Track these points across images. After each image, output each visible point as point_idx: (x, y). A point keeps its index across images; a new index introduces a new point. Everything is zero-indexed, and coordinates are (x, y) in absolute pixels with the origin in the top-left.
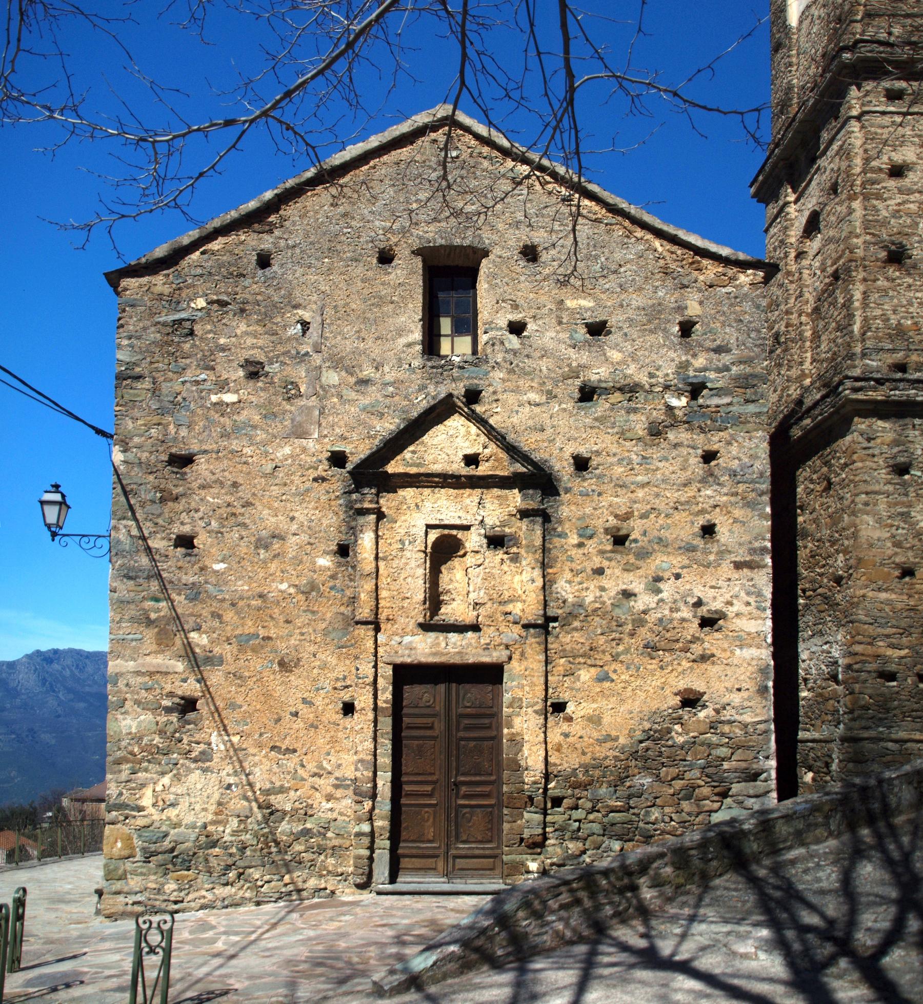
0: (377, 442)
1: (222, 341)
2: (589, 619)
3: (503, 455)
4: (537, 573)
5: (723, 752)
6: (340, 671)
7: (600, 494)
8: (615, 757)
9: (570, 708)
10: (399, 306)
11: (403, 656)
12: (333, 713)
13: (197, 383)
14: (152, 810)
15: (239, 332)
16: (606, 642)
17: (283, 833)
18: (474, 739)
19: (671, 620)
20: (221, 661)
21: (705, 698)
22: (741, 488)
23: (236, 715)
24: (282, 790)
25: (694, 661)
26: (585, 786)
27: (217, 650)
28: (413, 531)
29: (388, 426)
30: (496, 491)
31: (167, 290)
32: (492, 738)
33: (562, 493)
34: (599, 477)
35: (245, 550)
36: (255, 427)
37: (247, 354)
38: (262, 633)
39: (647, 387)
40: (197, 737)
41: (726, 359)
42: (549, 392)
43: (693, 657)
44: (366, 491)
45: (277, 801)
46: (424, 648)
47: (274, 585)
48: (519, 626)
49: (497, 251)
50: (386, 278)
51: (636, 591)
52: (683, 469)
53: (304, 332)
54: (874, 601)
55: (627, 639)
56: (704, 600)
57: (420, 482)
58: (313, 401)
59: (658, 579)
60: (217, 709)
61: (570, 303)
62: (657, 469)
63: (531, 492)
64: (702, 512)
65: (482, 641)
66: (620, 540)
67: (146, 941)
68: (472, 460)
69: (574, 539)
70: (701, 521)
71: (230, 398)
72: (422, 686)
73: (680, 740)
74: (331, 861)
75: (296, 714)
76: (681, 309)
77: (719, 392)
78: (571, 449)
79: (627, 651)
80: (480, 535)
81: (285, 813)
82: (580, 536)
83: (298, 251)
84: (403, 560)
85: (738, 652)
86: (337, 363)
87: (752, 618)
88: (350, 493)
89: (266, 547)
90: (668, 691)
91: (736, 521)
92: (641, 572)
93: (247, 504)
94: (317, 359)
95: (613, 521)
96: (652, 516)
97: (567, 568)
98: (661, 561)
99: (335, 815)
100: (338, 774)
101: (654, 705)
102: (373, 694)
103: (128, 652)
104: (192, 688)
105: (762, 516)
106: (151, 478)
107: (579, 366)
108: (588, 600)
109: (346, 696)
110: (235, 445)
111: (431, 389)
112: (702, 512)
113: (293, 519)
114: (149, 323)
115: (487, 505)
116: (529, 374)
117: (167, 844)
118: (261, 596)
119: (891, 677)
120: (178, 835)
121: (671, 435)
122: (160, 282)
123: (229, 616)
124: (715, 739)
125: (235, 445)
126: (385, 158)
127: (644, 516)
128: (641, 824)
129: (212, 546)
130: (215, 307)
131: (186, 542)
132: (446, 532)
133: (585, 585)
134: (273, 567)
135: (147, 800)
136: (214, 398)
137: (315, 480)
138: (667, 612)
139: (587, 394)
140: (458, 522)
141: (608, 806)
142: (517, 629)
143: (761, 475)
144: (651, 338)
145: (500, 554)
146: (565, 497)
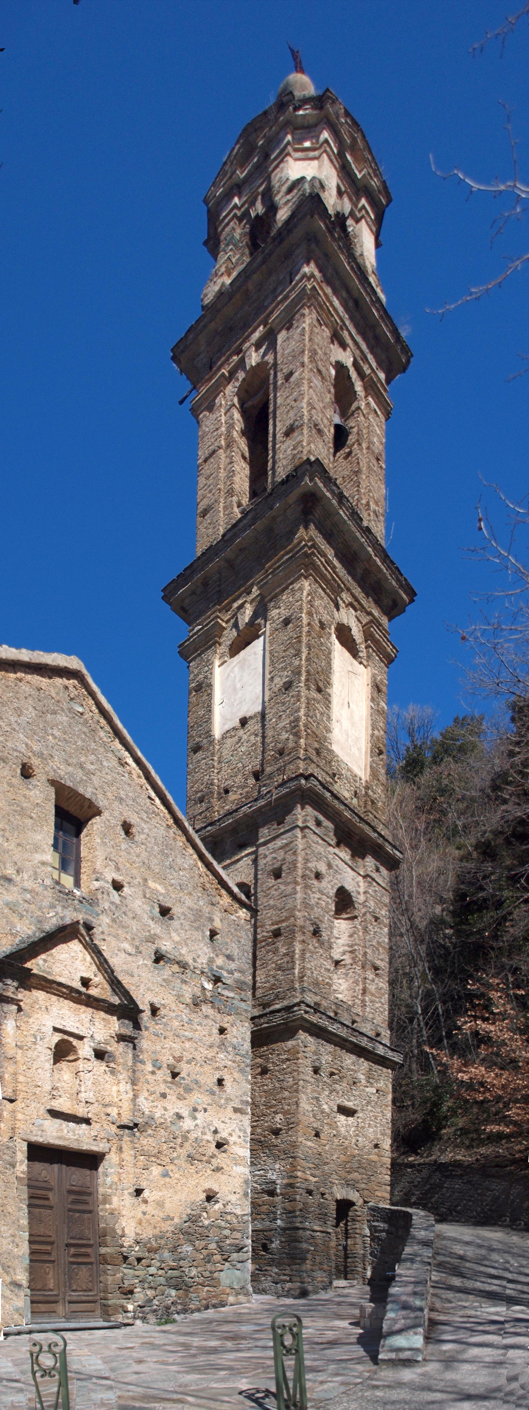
0: (17, 941)
2: (158, 1129)
3: (107, 986)
4: (129, 1087)
5: (227, 1232)
7: (165, 1038)
8: (172, 1231)
9: (146, 1194)
11: (37, 1136)
16: (167, 1149)
18: (79, 1211)
19: (202, 1140)
21: (218, 1196)
22: (238, 1058)
25: (213, 1170)
26: (155, 1251)
30: (102, 1014)
32: (90, 1212)
33: (143, 1029)
34: (165, 1025)
39: (192, 967)
41: (233, 966)
42: (137, 948)
43: (212, 1168)
48: (115, 1127)
49: (106, 815)
50: (27, 792)
51: (184, 1115)
54: (305, 1146)
56: (219, 1130)
57: (51, 988)
59: (195, 1110)
61: (151, 884)
62: (196, 1030)
63: (127, 1022)
64: (218, 1068)
65: (93, 1134)
66: (175, 1075)
67: (39, 1365)
68: (86, 982)
69: (149, 1067)
72: (41, 1164)
73: (206, 1222)
76: (211, 920)
80: (90, 1047)
82: (154, 1066)
84: (36, 1053)
85: (234, 1168)
90: (200, 1189)
91: (235, 1080)
95: (172, 1061)
96: (193, 1063)
97: (145, 1088)
98: (199, 1098)
105: (247, 1080)
107: (155, 935)
108: (157, 1115)
111: (59, 909)
112: (218, 1068)
115: (96, 1023)
116: (123, 927)
121: (204, 1008)
124: (223, 1224)
128: (186, 1279)
132: (66, 1037)
133: (155, 1104)
138: (200, 1134)
139: (159, 958)
140: (76, 1031)
141: (168, 1265)
142: (114, 1129)
144: (196, 933)
146: (144, 1033)
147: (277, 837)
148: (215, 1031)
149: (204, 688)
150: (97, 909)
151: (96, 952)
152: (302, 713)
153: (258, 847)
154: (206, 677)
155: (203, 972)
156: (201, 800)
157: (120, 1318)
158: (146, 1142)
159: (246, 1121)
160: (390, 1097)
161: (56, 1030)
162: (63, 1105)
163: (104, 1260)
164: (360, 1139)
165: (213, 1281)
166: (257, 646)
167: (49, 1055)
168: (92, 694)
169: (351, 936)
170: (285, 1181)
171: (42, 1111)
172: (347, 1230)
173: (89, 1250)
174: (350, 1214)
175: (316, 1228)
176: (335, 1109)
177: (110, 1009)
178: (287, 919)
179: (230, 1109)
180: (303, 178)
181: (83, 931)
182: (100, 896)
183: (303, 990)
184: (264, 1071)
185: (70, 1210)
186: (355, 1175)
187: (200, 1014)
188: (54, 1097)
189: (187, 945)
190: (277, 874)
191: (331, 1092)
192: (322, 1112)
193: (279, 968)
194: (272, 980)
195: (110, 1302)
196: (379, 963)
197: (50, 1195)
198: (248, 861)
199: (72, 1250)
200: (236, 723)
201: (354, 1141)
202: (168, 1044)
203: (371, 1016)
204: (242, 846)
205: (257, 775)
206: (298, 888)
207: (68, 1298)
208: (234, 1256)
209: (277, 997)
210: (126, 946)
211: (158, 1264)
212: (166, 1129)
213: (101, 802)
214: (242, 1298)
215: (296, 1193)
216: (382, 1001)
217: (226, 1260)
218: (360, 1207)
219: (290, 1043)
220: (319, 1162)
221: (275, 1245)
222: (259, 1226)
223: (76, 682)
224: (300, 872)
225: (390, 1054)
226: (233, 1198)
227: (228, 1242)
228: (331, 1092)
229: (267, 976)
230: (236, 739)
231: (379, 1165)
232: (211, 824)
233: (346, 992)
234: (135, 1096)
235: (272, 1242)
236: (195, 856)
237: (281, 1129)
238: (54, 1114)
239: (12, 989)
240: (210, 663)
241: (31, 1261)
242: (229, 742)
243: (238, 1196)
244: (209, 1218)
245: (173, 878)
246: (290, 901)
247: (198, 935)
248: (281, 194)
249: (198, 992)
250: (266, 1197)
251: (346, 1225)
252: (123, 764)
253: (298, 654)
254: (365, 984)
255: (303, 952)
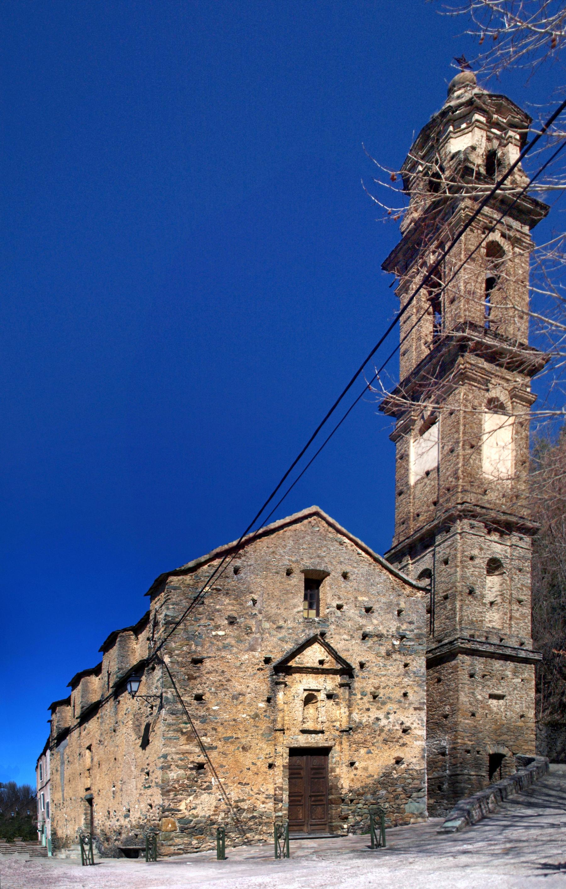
1: (217, 607)
3: (334, 661)
4: (346, 709)
5: (410, 781)
6: (268, 751)
9: (357, 764)
10: (295, 594)
12: (265, 768)
13: (205, 626)
14: (185, 811)
15: (225, 603)
17: (244, 818)
19: (393, 730)
20: (216, 748)
22: (417, 678)
23: (223, 770)
24: (243, 800)
27: (214, 744)
28: (298, 692)
29: (289, 647)
30: (331, 676)
31: (191, 582)
32: (324, 778)
34: (369, 671)
35: (227, 700)
36: (232, 646)
37: (229, 613)
38: (235, 736)
40: (205, 780)
41: (413, 627)
42: (351, 635)
44: (280, 674)
45: (240, 804)
46: (303, 741)
47: (240, 715)
49: (333, 574)
50: (289, 582)
52: (398, 670)
53: (254, 604)
54: (464, 723)
55: (377, 737)
58: (258, 635)
59: (388, 713)
60: (213, 769)
61: (360, 599)
64: (403, 687)
66: (375, 697)
68: (321, 662)
69: (359, 696)
70: (403, 691)
71: (221, 633)
73: (395, 776)
74: (265, 828)
75: (249, 769)
76: (398, 605)
77: (410, 640)
78: (359, 659)
79: (377, 742)
81: (244, 810)
83: (252, 567)
86: (268, 618)
87: (420, 729)
88: (273, 675)
89: (237, 699)
90: (391, 758)
91: (415, 692)
92: (382, 710)
93: (229, 680)
94: (260, 617)
95: (373, 689)
98: (390, 706)
99: (266, 810)
100: (267, 793)
101: (387, 763)
102: (282, 760)
103: (172, 744)
104: (202, 759)
105: (423, 690)
106: (183, 669)
108: (364, 721)
109: (270, 761)
110: (223, 654)
111: (307, 631)
112: (403, 687)
113: (248, 687)
114: (182, 598)
116: (344, 627)
117: (192, 824)
118: (234, 720)
119: (468, 752)
120: (198, 821)
122: (188, 578)
123: (220, 729)
124: (407, 776)
125: (223, 654)
126: (290, 528)
127: (384, 688)
129: (212, 699)
130: (214, 591)
131: (199, 698)
134: (240, 707)
135: (182, 806)
136: (214, 633)
137: (258, 670)
139: (365, 636)
140: (316, 688)
142: (338, 733)
143: (424, 674)
144: (388, 616)
145: (332, 702)
146: (356, 679)
147: (446, 540)
148: (401, 667)
149: (405, 457)
150: (328, 623)
151: (327, 646)
152: (460, 465)
153: (436, 547)
154: (405, 451)
155: (393, 636)
156: (403, 523)
157: (340, 832)
158: (357, 737)
159: (423, 715)
160: (533, 683)
161: (305, 690)
162: (309, 726)
163: (331, 802)
164: (508, 713)
165: (399, 810)
166: (434, 430)
167: (302, 703)
168: (324, 519)
169: (501, 585)
170: (451, 746)
171: (297, 731)
172: (501, 773)
173: (322, 798)
174: (503, 762)
175: (473, 773)
176: (487, 697)
177: (335, 672)
178: (451, 588)
179: (411, 709)
180: (459, 152)
181: (320, 638)
182: (329, 616)
183: (461, 630)
184: (439, 680)
185: (312, 778)
186: (505, 737)
187: (391, 659)
188: (304, 722)
189: (382, 624)
190: (446, 562)
191: (483, 687)
192: (477, 700)
193: (447, 618)
194: (443, 626)
195: (334, 824)
196: (522, 597)
197: (302, 772)
198: (430, 555)
199: (313, 799)
200: (424, 475)
201: (504, 714)
202: (371, 681)
203: (516, 633)
204: (426, 547)
205: (435, 503)
206: (458, 569)
207: (310, 823)
208: (414, 794)
209: (446, 635)
210: (345, 637)
211: (364, 802)
212: (369, 728)
213: (330, 568)
214: (420, 820)
215: (457, 753)
216: (526, 621)
217: (409, 797)
218: (510, 757)
219: (453, 662)
220: (475, 732)
221: (445, 786)
222: (430, 777)
223: (318, 507)
224: (459, 559)
225: (531, 656)
226: (414, 760)
227: (410, 786)
228: (483, 687)
229: (441, 623)
230: (423, 484)
231: (525, 728)
232: (408, 538)
233: (498, 621)
234: (350, 714)
235: (443, 784)
236: (388, 573)
237: (448, 715)
238: (304, 732)
239: (282, 677)
240: (407, 442)
241: (289, 805)
242: (419, 486)
243: (417, 759)
244: (397, 773)
245: (373, 590)
246: (453, 577)
247: (390, 616)
248: (446, 161)
249: (390, 647)
250: (441, 757)
251: (500, 770)
252: (341, 544)
253: (457, 432)
254: (511, 613)
255: (461, 606)
